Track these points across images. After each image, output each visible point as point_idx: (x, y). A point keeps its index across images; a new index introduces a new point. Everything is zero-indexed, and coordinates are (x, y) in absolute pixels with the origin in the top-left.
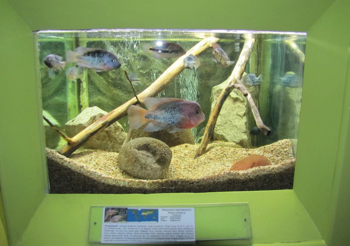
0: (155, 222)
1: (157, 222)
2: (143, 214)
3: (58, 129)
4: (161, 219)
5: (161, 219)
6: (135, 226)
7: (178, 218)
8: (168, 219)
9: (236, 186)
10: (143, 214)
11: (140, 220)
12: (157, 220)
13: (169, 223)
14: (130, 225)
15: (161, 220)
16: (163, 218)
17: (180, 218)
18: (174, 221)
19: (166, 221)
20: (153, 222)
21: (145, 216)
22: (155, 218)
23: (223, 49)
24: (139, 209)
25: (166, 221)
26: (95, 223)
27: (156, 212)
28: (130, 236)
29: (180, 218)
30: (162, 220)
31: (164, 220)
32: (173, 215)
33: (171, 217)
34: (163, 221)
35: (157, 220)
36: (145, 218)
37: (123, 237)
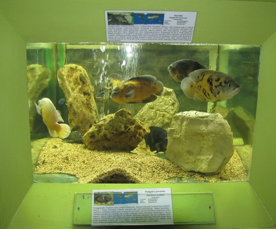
0: (136, 204)
2: (149, 18)
4: (140, 201)
5: (140, 201)
6: (184, 40)
7: (155, 200)
8: (146, 201)
10: (126, 196)
12: (137, 202)
13: (147, 204)
16: (167, 22)
17: (156, 200)
18: (151, 202)
21: (127, 198)
23: (88, 73)
27: (162, 16)
29: (156, 200)
30: (141, 202)
31: (143, 202)
32: (152, 197)
33: (149, 199)
34: (142, 203)
36: (127, 200)
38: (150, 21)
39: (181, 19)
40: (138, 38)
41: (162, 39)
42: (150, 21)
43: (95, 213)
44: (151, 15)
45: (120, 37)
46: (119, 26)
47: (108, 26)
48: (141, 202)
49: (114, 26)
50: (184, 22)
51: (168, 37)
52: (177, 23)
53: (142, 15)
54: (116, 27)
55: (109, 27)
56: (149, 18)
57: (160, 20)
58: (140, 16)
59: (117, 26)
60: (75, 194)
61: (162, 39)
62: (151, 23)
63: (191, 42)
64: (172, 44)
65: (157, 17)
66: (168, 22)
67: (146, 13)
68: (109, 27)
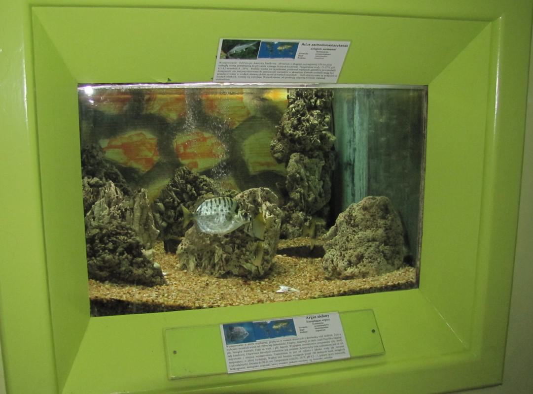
2: (275, 327)
10: (279, 48)
14: (269, 62)
15: (298, 58)
16: (302, 329)
19: (306, 332)
20: (288, 59)
22: (292, 54)
24: (269, 322)
25: (306, 332)
26: (175, 352)
27: (290, 323)
30: (302, 331)
35: (293, 57)
38: (280, 53)
42: (280, 53)
46: (242, 345)
47: (227, 347)
48: (302, 331)
49: (235, 346)
54: (237, 346)
55: (228, 348)
56: (275, 327)
58: (262, 327)
59: (239, 346)
60: (82, 102)
62: (279, 335)
63: (335, 80)
66: (304, 55)
68: (228, 348)
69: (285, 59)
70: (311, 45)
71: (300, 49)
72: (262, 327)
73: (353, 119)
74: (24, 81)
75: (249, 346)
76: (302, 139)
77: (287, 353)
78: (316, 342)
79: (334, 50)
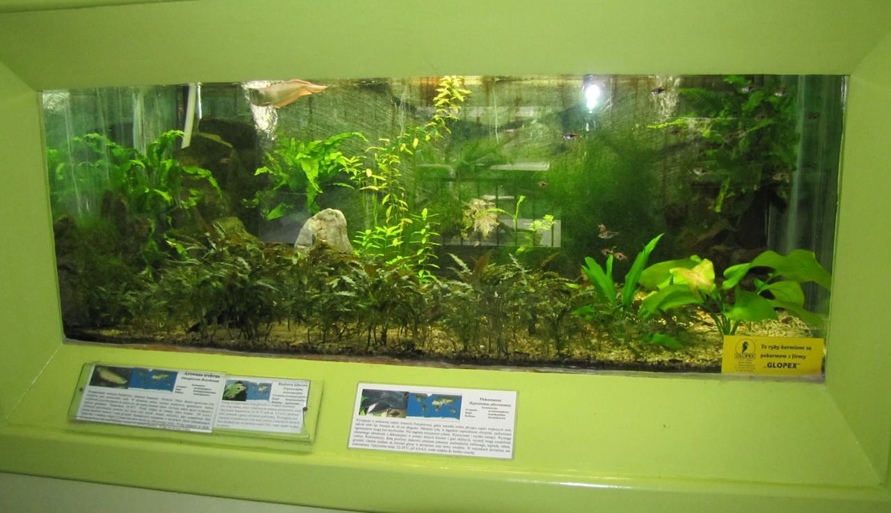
0: (455, 419)
1: (457, 420)
2: (435, 403)
3: (65, 216)
9: (730, 118)
11: (428, 415)
12: (457, 416)
16: (277, 397)
19: (214, 393)
20: (451, 419)
21: (155, 380)
24: (429, 395)
27: (457, 400)
28: (101, 397)
30: (468, 415)
31: (278, 401)
34: (469, 416)
35: (457, 416)
37: (472, 439)
39: (496, 407)
40: (484, 448)
41: (177, 403)
42: (437, 410)
43: (88, 397)
44: (439, 397)
45: (503, 447)
48: (468, 415)
50: (500, 413)
51: (358, 430)
52: (488, 416)
53: (423, 397)
56: (435, 403)
57: (455, 409)
58: (419, 400)
61: (177, 403)
64: (514, 480)
65: (450, 403)
66: (280, 397)
67: (429, 391)
69: (446, 419)
70: (805, 348)
71: (179, 381)
72: (419, 400)
73: (112, 337)
74: (572, 486)
75: (232, 405)
76: (468, 108)
77: (403, 431)
78: (434, 444)
79: (218, 381)
